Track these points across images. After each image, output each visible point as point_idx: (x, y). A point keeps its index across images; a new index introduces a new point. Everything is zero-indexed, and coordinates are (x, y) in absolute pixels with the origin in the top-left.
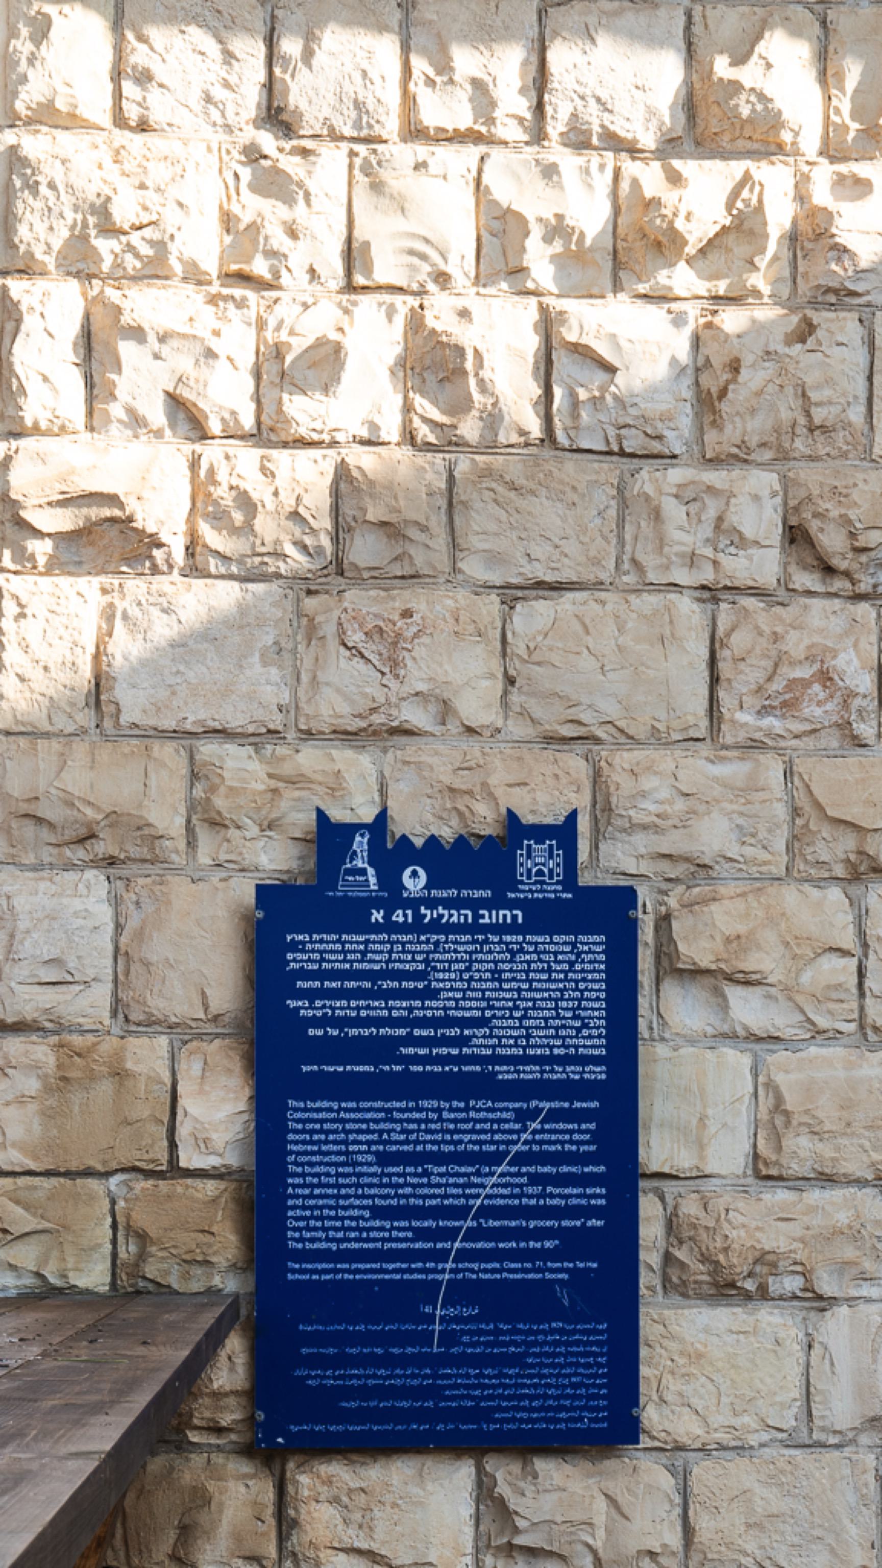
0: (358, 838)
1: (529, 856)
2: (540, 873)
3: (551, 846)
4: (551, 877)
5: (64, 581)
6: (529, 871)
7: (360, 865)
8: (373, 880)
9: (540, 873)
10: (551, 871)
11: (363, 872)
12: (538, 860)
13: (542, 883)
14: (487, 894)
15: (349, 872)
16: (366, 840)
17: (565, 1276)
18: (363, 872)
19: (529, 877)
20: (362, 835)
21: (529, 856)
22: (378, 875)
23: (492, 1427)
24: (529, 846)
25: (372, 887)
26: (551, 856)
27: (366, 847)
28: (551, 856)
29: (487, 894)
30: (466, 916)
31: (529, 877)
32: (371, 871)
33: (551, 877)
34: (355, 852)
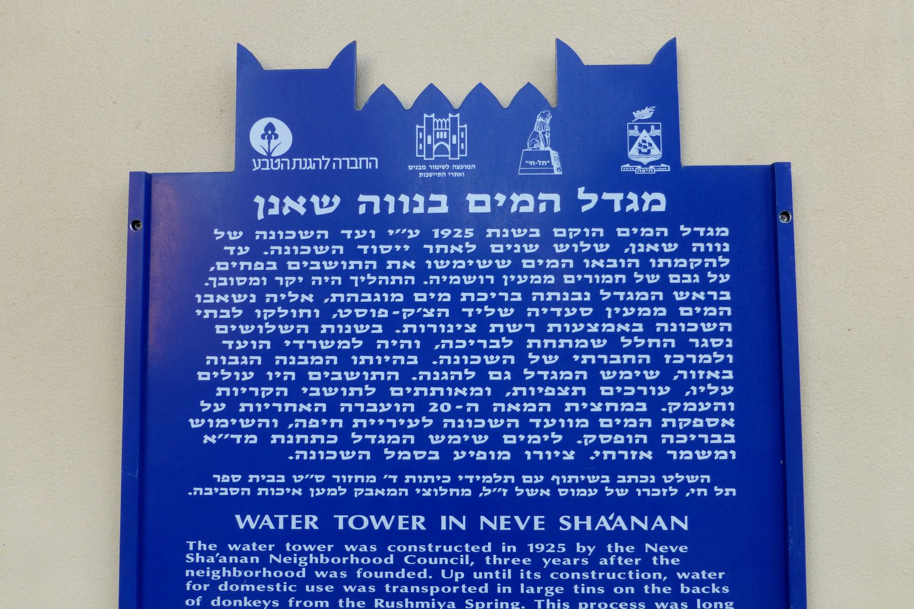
0: (539, 119)
1: (429, 132)
2: (441, 149)
3: (454, 120)
4: (454, 154)
6: (429, 148)
8: (556, 165)
9: (441, 149)
10: (454, 147)
11: (546, 155)
13: (446, 161)
14: (370, 162)
15: (529, 156)
16: (548, 121)
18: (546, 155)
19: (429, 154)
20: (544, 116)
21: (429, 132)
22: (562, 159)
23: (210, 492)
24: (429, 121)
25: (556, 173)
26: (454, 132)
27: (548, 129)
28: (454, 132)
29: (370, 162)
30: (550, 204)
32: (554, 154)
33: (454, 154)
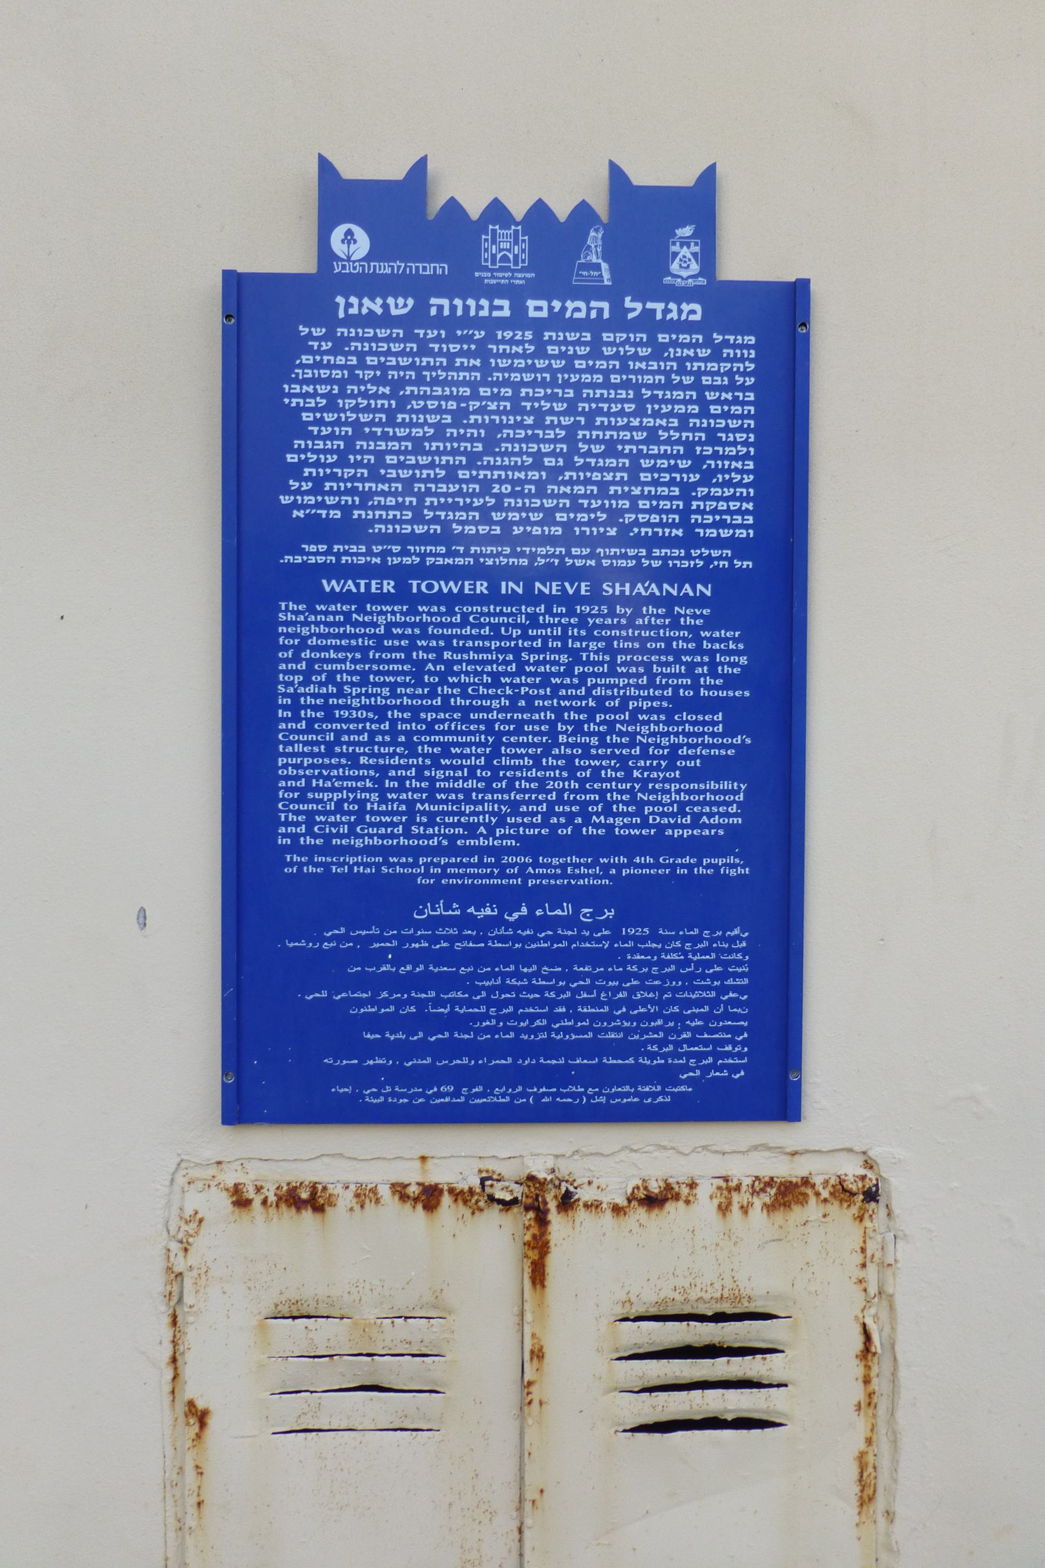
0: (592, 234)
1: (494, 242)
2: (505, 259)
3: (516, 232)
4: (516, 263)
5: (317, 160)
6: (494, 256)
7: (595, 260)
8: (606, 275)
9: (505, 259)
10: (516, 257)
11: (598, 267)
12: (503, 245)
14: (441, 268)
15: (583, 267)
16: (600, 235)
17: (731, 752)
19: (494, 263)
20: (596, 231)
21: (494, 242)
22: (612, 270)
24: (494, 231)
25: (606, 283)
26: (516, 242)
27: (600, 243)
28: (516, 242)
29: (441, 268)
30: (600, 311)
31: (494, 263)
32: (604, 266)
33: (516, 263)
34: (589, 247)
